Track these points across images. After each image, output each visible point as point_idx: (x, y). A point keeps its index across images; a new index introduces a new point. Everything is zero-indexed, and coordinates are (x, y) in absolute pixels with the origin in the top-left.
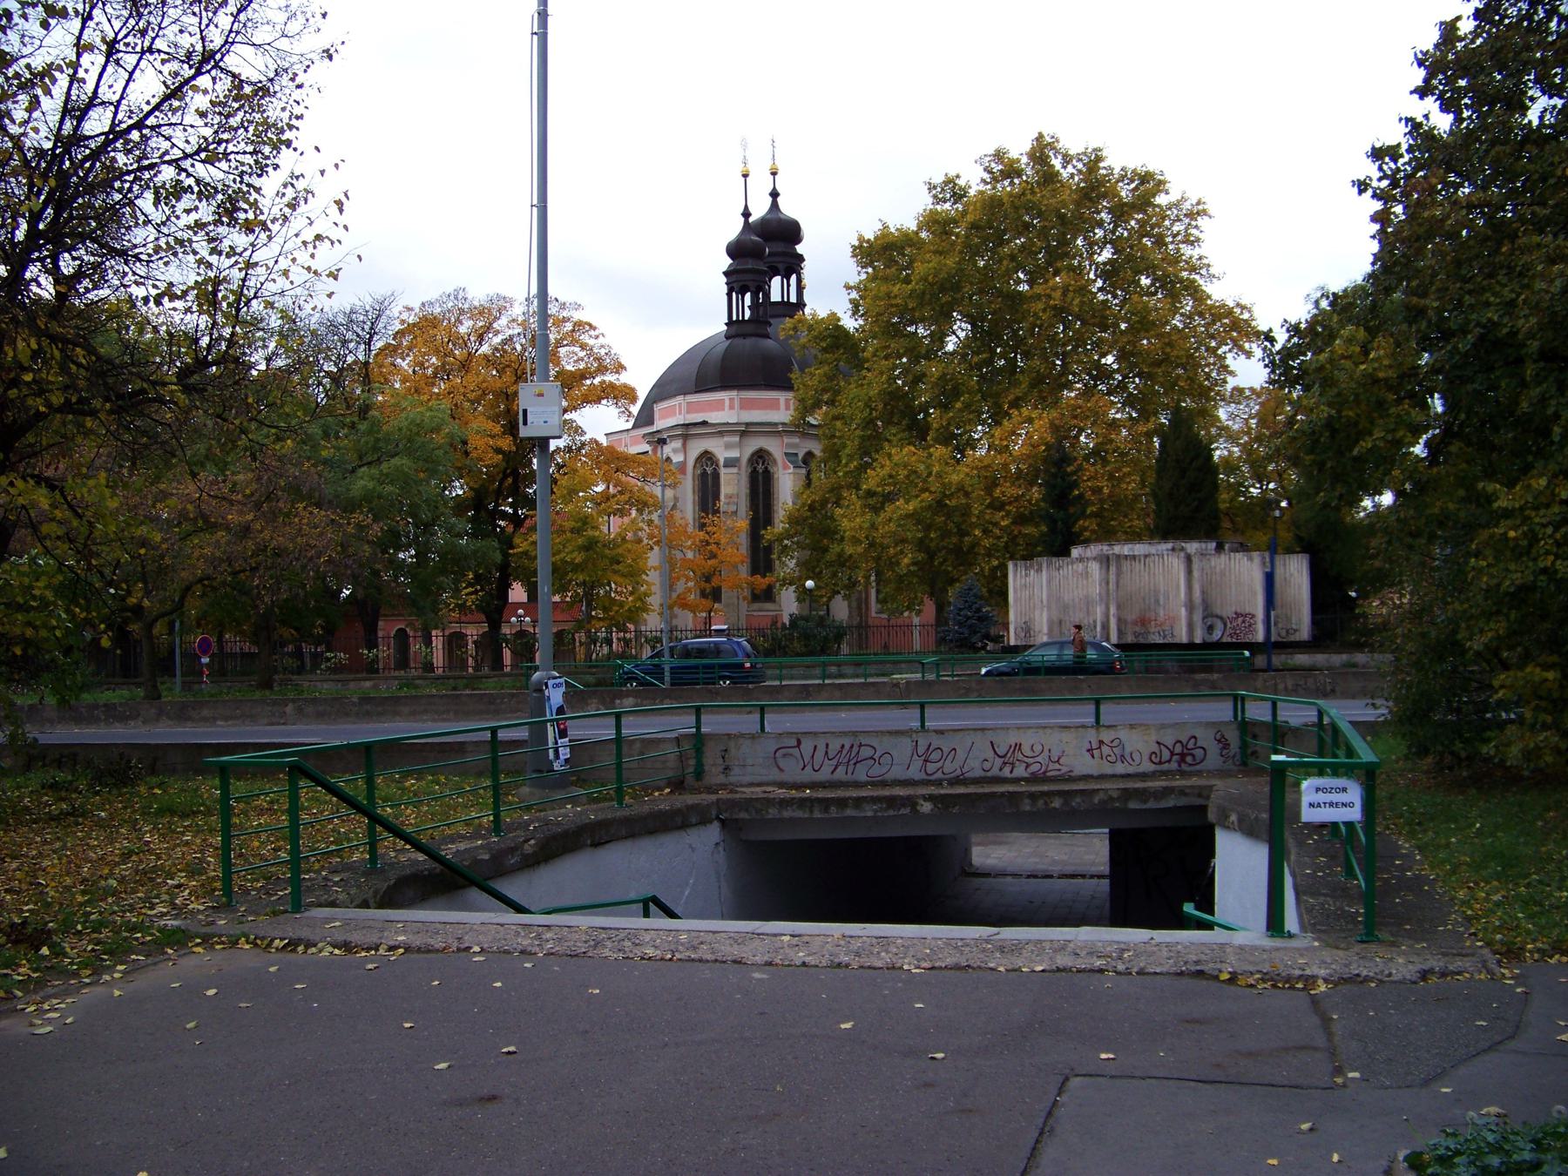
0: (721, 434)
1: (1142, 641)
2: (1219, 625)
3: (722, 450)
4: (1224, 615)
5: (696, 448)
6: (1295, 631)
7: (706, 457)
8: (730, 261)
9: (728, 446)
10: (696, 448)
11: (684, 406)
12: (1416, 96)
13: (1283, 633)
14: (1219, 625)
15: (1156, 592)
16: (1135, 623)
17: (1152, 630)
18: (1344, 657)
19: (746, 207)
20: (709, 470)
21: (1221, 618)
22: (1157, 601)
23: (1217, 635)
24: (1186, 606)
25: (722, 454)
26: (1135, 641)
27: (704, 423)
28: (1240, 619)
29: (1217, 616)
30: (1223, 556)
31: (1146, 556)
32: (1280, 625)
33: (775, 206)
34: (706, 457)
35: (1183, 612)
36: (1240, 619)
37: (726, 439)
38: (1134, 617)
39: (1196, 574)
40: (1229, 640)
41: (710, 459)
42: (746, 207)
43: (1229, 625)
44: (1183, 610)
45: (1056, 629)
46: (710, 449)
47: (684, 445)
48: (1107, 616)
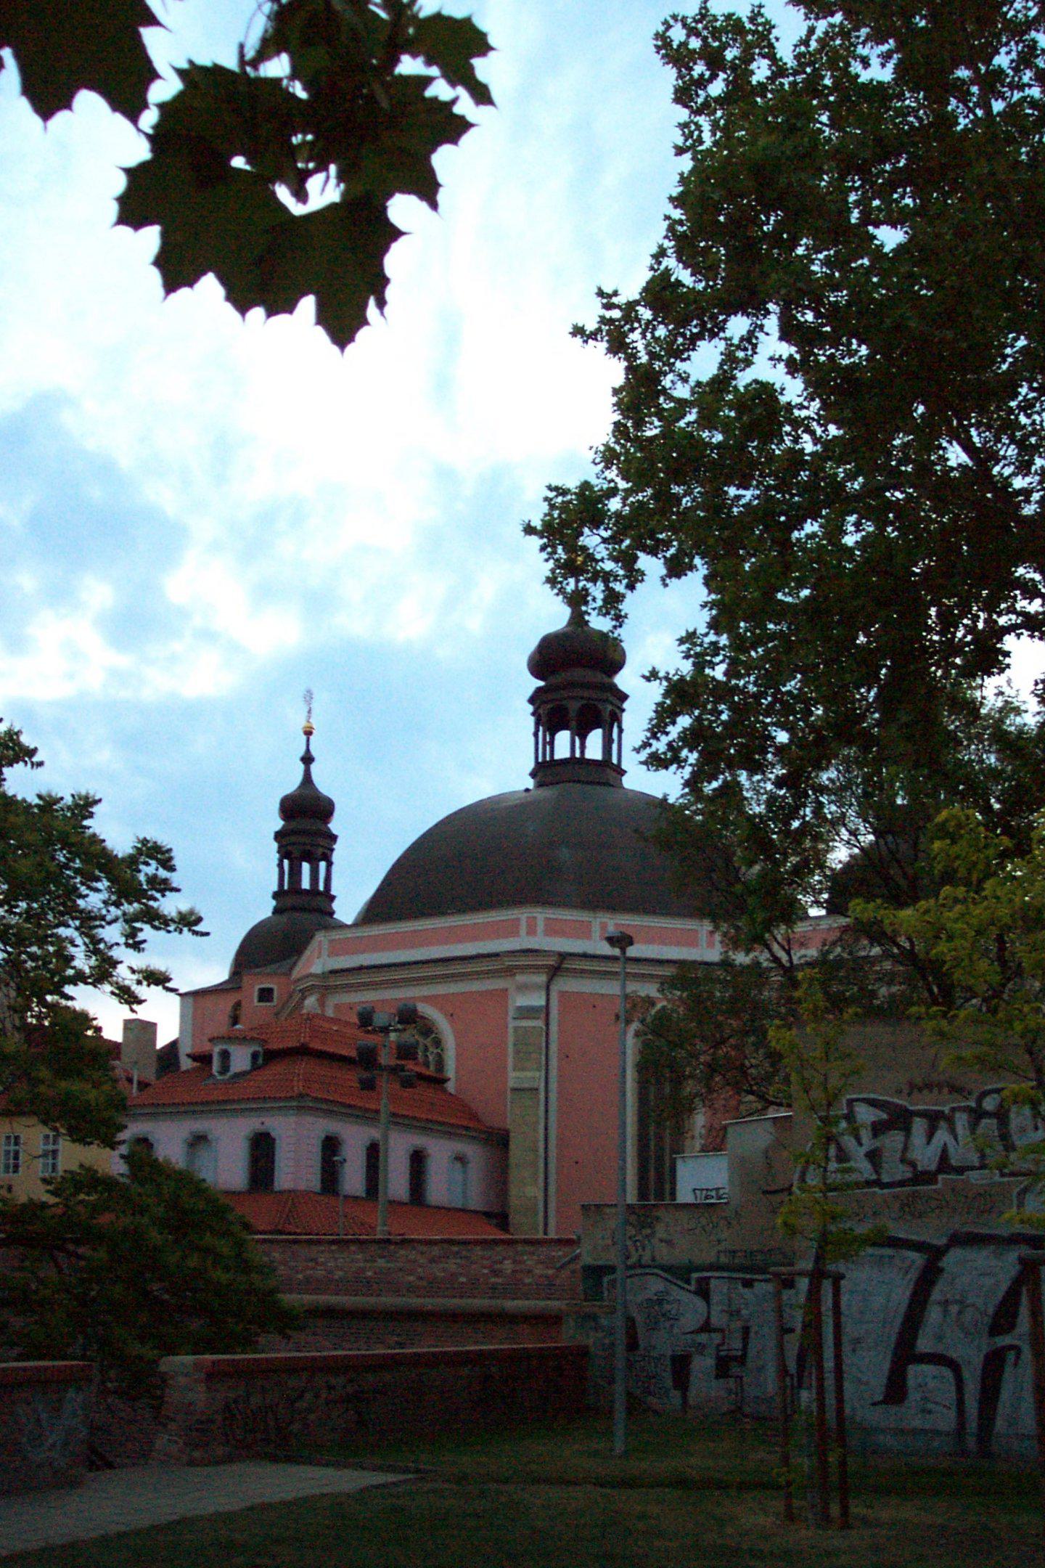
12: (596, 291)
19: (308, 750)
33: (307, 778)
42: (308, 750)
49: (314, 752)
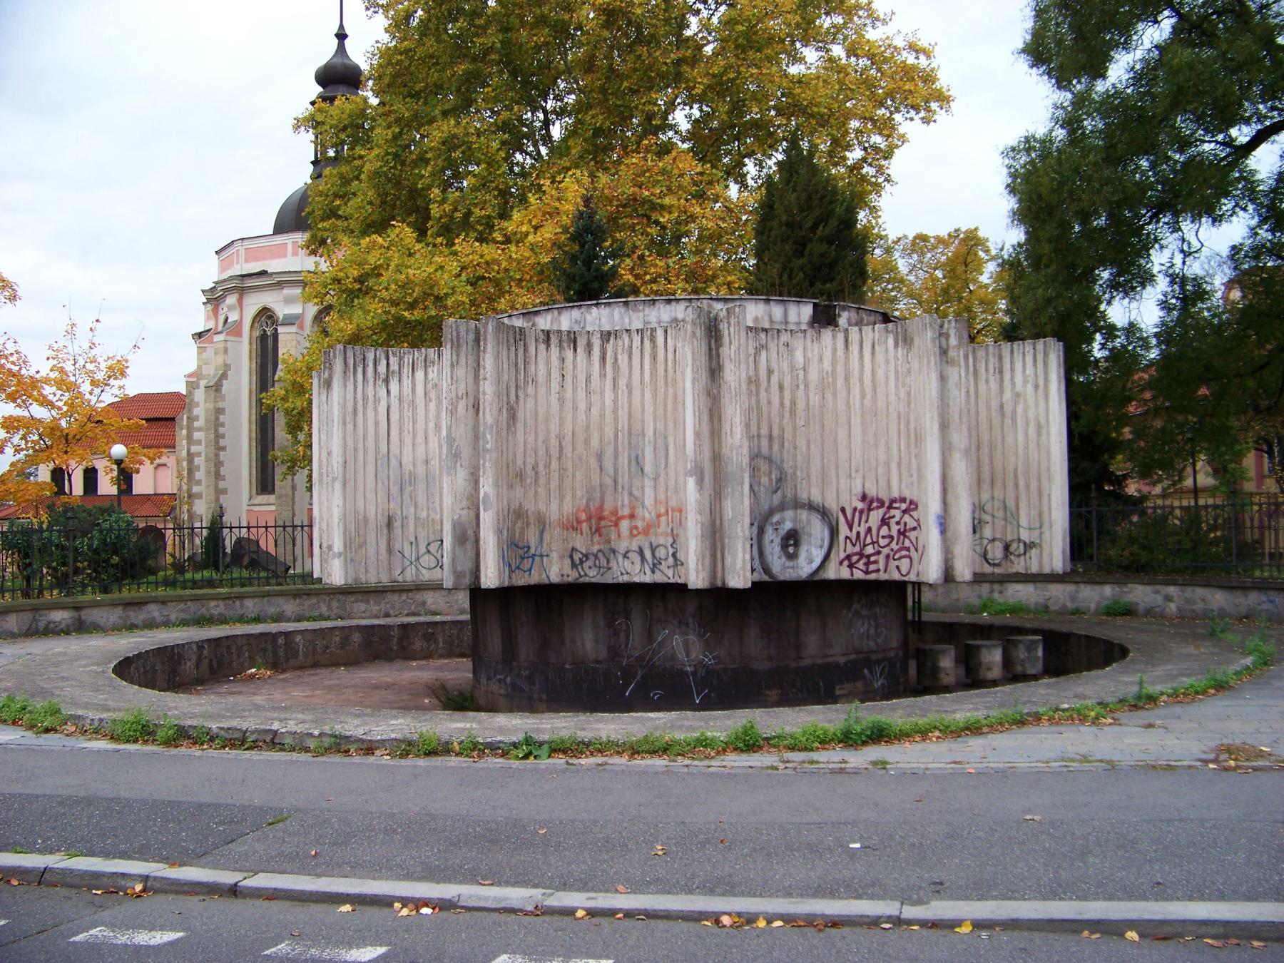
0: (280, 285)
1: (592, 575)
2: (816, 531)
3: (284, 304)
4: (832, 505)
5: (254, 303)
6: (1028, 546)
7: (265, 314)
8: (320, 89)
9: (288, 301)
10: (254, 303)
11: (242, 253)
13: (996, 552)
14: (816, 531)
15: (635, 435)
16: (573, 526)
17: (622, 546)
18: (1108, 590)
19: (341, 26)
20: (269, 331)
21: (824, 513)
22: (638, 462)
23: (805, 565)
24: (699, 473)
25: (281, 311)
26: (572, 576)
27: (263, 273)
28: (876, 517)
29: (811, 507)
30: (827, 334)
31: (606, 336)
32: (988, 532)
33: (341, 49)
34: (265, 314)
35: (691, 493)
36: (876, 517)
37: (287, 291)
38: (568, 507)
39: (733, 374)
40: (845, 574)
41: (271, 317)
42: (341, 26)
43: (844, 530)
44: (691, 483)
45: (375, 543)
46: (270, 305)
47: (240, 301)
48: (474, 505)
49: (348, 31)
